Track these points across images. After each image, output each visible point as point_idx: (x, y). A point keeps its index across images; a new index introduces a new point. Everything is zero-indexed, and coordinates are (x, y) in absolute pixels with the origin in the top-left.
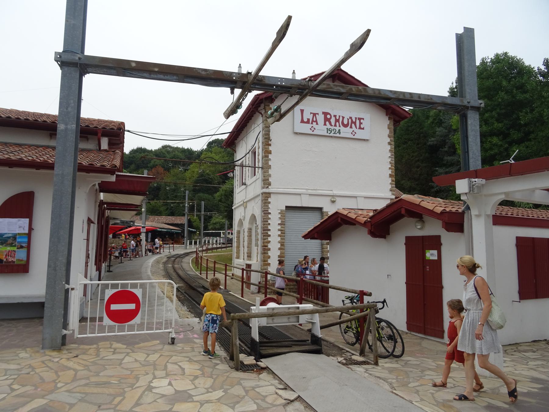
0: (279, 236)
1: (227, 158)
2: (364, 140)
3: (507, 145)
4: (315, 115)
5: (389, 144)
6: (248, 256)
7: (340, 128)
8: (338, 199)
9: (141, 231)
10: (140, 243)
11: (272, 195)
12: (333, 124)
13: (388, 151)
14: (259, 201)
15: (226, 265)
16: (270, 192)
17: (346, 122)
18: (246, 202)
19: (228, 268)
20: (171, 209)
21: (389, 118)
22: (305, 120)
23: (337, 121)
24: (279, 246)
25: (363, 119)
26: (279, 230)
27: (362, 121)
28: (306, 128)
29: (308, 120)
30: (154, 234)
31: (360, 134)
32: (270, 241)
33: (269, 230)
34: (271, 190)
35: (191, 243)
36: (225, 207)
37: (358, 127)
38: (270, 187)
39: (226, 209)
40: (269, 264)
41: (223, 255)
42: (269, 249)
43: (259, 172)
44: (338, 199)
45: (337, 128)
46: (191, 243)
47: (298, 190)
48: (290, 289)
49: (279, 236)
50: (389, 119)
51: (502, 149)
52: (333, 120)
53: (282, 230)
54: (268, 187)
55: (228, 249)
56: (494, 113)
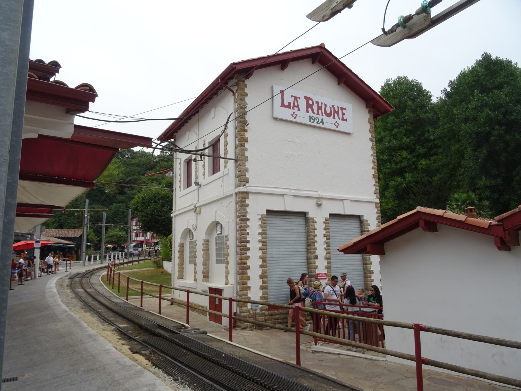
0: (260, 249)
1: (123, 169)
2: (347, 133)
3: (414, 159)
4: (296, 98)
5: (371, 140)
6: (204, 277)
7: (323, 117)
8: (324, 202)
9: (35, 246)
10: (33, 262)
11: (250, 196)
12: (316, 112)
13: (370, 148)
14: (231, 204)
15: (161, 286)
16: (248, 191)
17: (328, 111)
18: (200, 207)
19: (163, 289)
20: (59, 222)
21: (369, 111)
22: (286, 104)
23: (319, 108)
24: (261, 263)
25: (345, 109)
26: (260, 241)
27: (344, 111)
28: (286, 114)
29: (289, 103)
30: (46, 250)
31: (343, 127)
32: (249, 257)
33: (248, 242)
34: (249, 188)
35: (90, 259)
36: (142, 216)
37: (341, 118)
38: (247, 185)
39: (144, 218)
40: (249, 288)
41: (138, 272)
42: (249, 268)
43: (228, 168)
44: (324, 202)
45: (320, 117)
46: (90, 259)
47: (280, 190)
48: (275, 319)
49: (260, 249)
50: (370, 112)
51: (411, 162)
52: (315, 107)
53: (263, 242)
54: (245, 185)
55: (140, 262)
56: (402, 129)
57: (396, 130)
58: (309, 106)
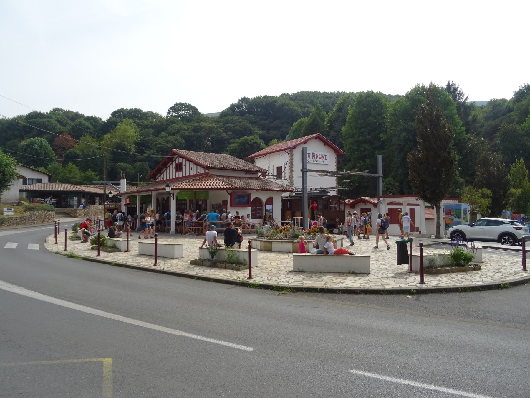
23: (317, 156)
52: (316, 156)
57: (362, 130)
58: (313, 156)
